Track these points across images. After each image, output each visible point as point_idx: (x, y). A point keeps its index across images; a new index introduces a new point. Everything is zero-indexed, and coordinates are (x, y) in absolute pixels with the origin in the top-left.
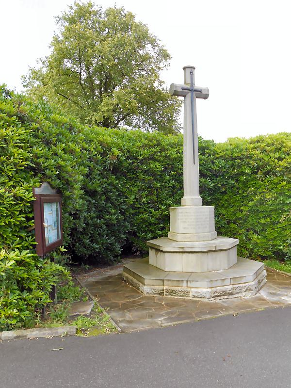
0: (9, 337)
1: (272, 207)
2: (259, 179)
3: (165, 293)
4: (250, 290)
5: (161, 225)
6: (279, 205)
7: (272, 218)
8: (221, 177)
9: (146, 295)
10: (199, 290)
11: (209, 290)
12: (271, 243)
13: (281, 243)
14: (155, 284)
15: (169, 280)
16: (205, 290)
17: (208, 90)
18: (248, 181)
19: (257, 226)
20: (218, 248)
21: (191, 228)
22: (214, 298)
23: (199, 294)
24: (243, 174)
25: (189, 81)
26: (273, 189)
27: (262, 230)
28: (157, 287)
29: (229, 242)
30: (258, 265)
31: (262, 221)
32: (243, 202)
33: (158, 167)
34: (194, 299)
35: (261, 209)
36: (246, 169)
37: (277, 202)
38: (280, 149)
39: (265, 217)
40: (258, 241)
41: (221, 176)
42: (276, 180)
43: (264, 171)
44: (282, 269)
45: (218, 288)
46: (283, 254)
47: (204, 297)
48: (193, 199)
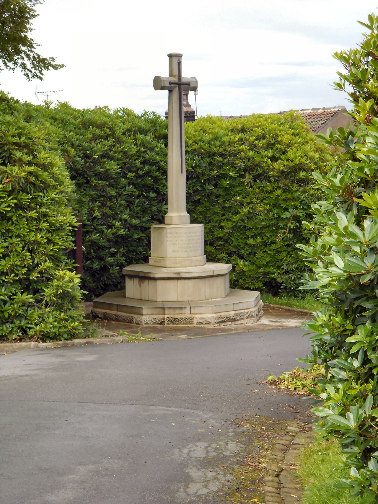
0: (108, 328)
1: (263, 223)
2: (248, 184)
3: (166, 322)
4: (252, 316)
5: (113, 249)
6: (272, 220)
7: (264, 237)
8: (194, 181)
9: (145, 326)
10: (204, 316)
11: (214, 315)
12: (262, 270)
13: (275, 270)
14: (155, 313)
15: (170, 308)
16: (210, 316)
17: (197, 82)
18: (232, 186)
19: (243, 248)
20: (215, 273)
21: (182, 251)
22: (218, 324)
23: (204, 320)
24: (225, 176)
25: (176, 72)
26: (264, 199)
27: (250, 253)
28: (157, 317)
29: (224, 268)
30: (258, 293)
31: (251, 242)
32: (224, 215)
33: (113, 167)
34: (198, 326)
35: (249, 225)
36: (229, 170)
37: (270, 216)
38: (274, 144)
39: (254, 237)
40: (245, 269)
41: (194, 178)
42: (269, 187)
43: (254, 173)
44: (277, 303)
45: (223, 314)
46: (277, 284)
47: (209, 323)
48: (181, 216)
